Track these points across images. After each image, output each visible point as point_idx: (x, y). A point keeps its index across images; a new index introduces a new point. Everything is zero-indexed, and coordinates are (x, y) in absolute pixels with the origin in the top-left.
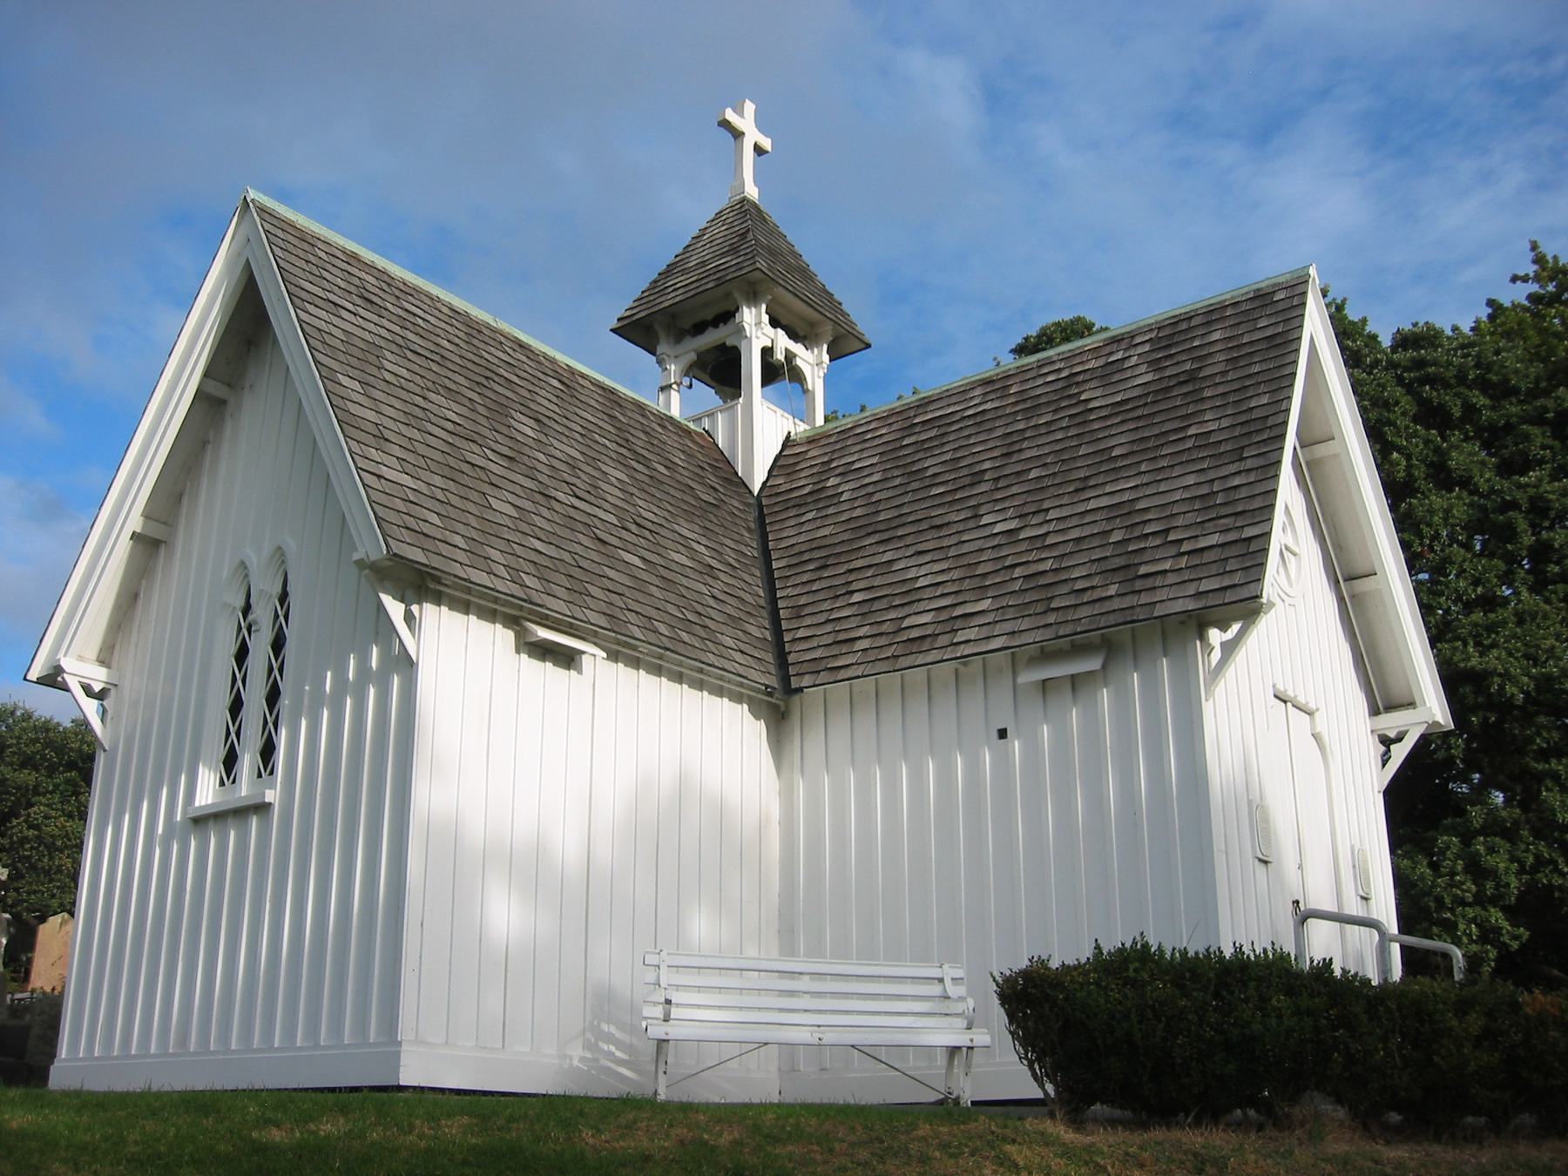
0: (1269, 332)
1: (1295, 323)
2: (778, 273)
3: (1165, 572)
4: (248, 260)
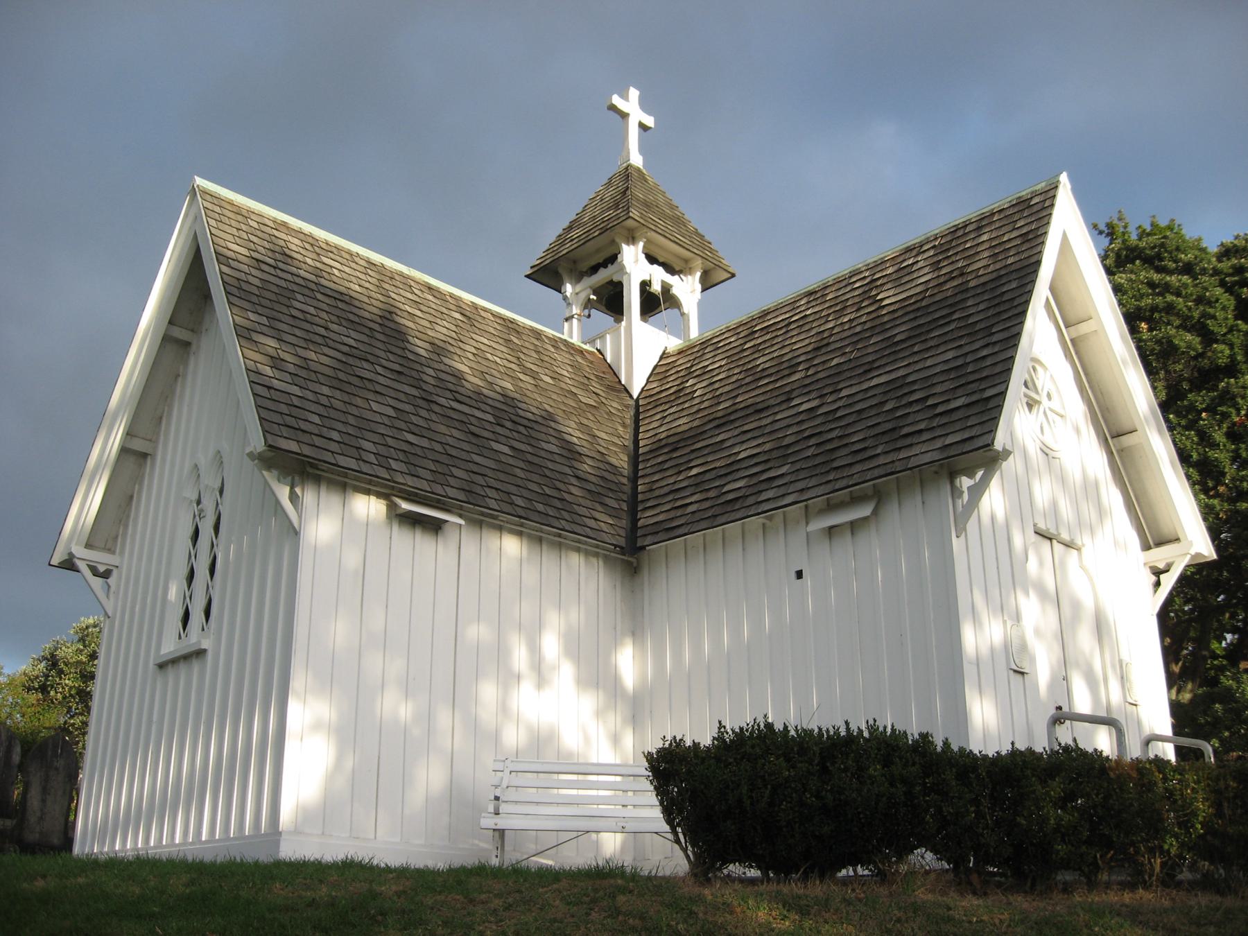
0: (1024, 230)
2: (650, 220)
3: (920, 431)
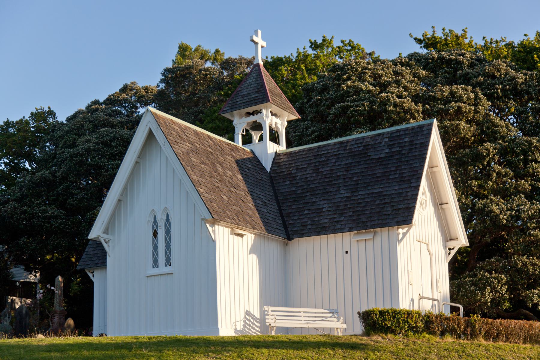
1: (409, 218)
4: (150, 128)
